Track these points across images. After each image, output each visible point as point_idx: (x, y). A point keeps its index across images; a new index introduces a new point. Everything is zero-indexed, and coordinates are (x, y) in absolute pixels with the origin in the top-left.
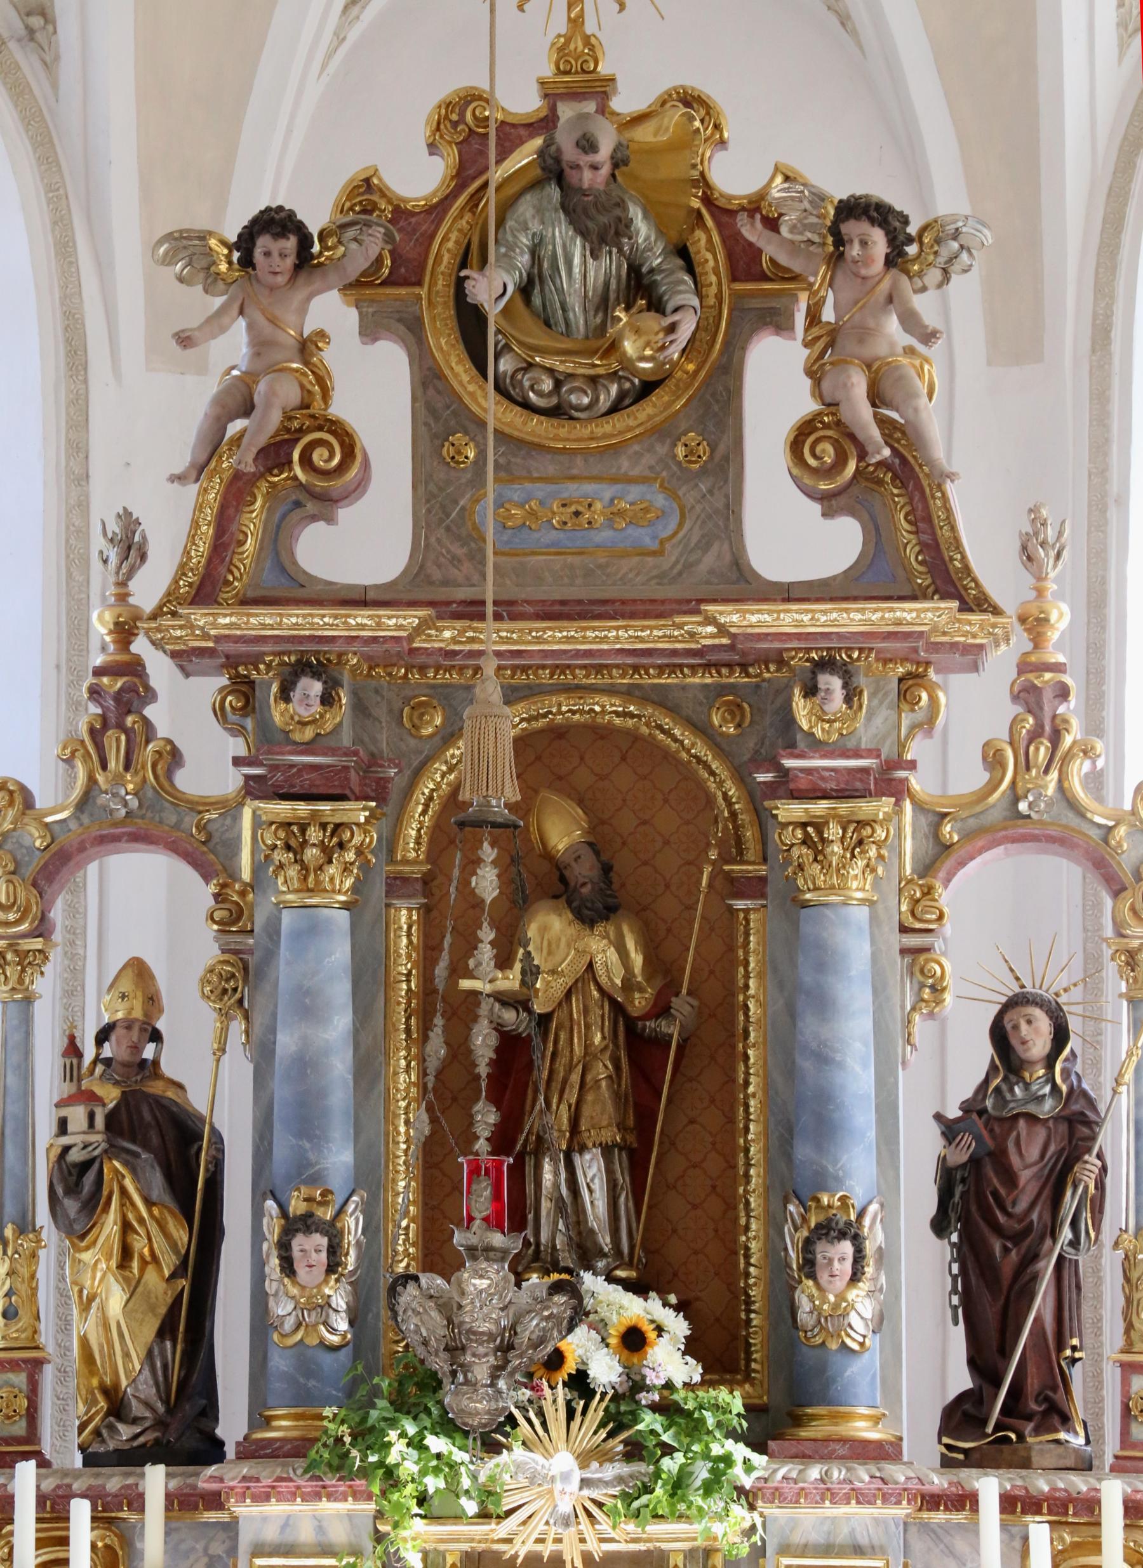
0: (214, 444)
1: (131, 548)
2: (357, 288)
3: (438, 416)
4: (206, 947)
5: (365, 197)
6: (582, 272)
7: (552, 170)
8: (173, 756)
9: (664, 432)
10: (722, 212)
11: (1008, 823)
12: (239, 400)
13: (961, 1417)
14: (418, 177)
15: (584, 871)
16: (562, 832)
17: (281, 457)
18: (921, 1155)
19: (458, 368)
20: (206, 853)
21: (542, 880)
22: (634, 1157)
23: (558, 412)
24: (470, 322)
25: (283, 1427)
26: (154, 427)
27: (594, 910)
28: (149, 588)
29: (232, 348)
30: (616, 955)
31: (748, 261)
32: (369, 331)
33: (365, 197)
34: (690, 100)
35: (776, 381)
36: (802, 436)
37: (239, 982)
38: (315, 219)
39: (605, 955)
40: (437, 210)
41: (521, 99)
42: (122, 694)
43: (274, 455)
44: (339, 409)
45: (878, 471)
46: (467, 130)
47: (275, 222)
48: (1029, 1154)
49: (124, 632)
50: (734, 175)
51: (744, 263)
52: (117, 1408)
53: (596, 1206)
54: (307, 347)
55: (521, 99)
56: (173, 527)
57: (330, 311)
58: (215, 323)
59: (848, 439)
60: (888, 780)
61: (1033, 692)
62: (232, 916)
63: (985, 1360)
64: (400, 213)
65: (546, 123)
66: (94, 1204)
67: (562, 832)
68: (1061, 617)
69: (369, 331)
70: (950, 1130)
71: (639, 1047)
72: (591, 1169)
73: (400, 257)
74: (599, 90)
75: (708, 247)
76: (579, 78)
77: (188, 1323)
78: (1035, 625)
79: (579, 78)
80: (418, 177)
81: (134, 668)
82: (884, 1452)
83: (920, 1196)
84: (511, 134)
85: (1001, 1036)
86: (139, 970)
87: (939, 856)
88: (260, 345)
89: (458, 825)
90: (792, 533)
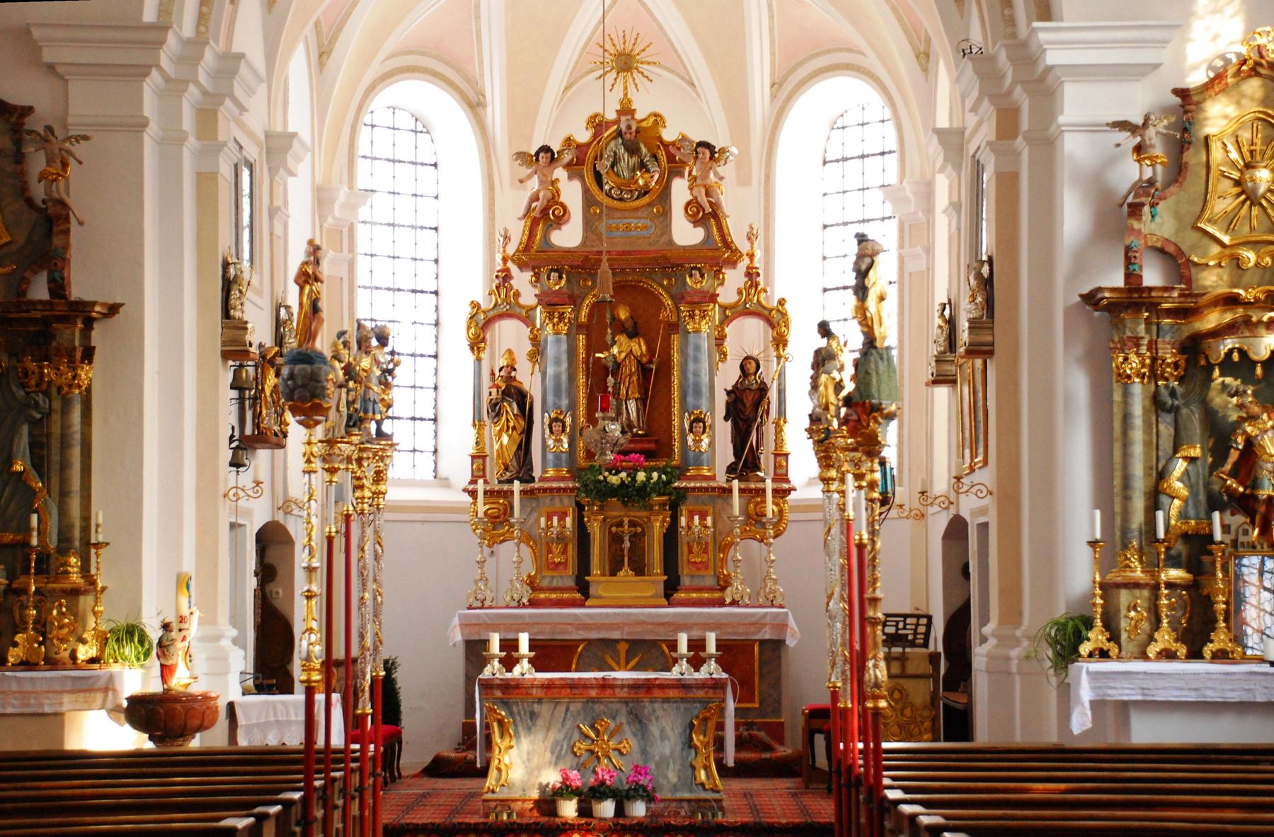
0: (529, 209)
1: (507, 238)
2: (568, 166)
3: (589, 201)
4: (528, 347)
5: (569, 141)
6: (626, 161)
7: (619, 134)
8: (517, 294)
9: (650, 205)
10: (666, 145)
11: (741, 310)
12: (535, 198)
13: (731, 469)
14: (583, 136)
15: (629, 324)
16: (623, 314)
17: (547, 214)
18: (721, 400)
19: (594, 188)
20: (528, 320)
21: (620, 328)
22: (642, 401)
23: (621, 199)
24: (598, 178)
25: (551, 473)
26: (515, 203)
27: (632, 336)
28: (511, 249)
29: (534, 184)
30: (639, 347)
31: (674, 158)
32: (570, 178)
33: (569, 141)
34: (656, 115)
35: (680, 191)
36: (688, 204)
37: (537, 352)
38: (556, 148)
39: (635, 348)
40: (588, 145)
41: (611, 115)
42: (505, 277)
43: (545, 211)
44: (562, 199)
45: (706, 213)
46: (598, 124)
47: (546, 149)
48: (749, 399)
49: (505, 260)
50: (669, 135)
51: (671, 158)
52: (506, 469)
53: (633, 415)
54: (554, 183)
55: (611, 115)
56: (518, 232)
57: (560, 173)
58: (530, 177)
59: (700, 207)
60: (713, 298)
61: (751, 274)
62: (535, 340)
63: (738, 453)
64: (579, 146)
65: (617, 122)
66: (498, 415)
67: (623, 314)
68: (758, 254)
69: (570, 178)
70: (729, 393)
71: (644, 370)
72: (632, 405)
73: (580, 159)
74: (631, 112)
75: (663, 159)
76: (626, 110)
77: (524, 448)
78: (751, 256)
79: (626, 110)
80: (583, 136)
81: (507, 270)
82: (713, 478)
83: (720, 410)
84: (609, 124)
85: (742, 367)
86: (510, 352)
87: (726, 320)
88: (541, 182)
89: (598, 306)
90: (686, 234)
